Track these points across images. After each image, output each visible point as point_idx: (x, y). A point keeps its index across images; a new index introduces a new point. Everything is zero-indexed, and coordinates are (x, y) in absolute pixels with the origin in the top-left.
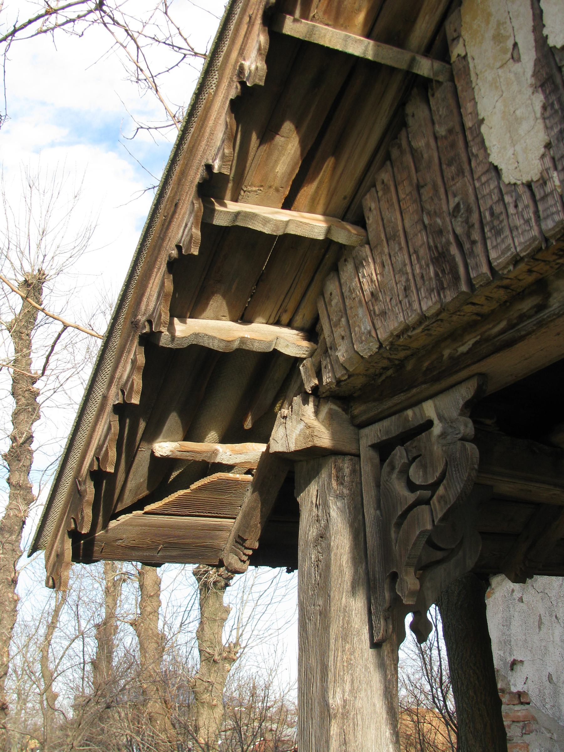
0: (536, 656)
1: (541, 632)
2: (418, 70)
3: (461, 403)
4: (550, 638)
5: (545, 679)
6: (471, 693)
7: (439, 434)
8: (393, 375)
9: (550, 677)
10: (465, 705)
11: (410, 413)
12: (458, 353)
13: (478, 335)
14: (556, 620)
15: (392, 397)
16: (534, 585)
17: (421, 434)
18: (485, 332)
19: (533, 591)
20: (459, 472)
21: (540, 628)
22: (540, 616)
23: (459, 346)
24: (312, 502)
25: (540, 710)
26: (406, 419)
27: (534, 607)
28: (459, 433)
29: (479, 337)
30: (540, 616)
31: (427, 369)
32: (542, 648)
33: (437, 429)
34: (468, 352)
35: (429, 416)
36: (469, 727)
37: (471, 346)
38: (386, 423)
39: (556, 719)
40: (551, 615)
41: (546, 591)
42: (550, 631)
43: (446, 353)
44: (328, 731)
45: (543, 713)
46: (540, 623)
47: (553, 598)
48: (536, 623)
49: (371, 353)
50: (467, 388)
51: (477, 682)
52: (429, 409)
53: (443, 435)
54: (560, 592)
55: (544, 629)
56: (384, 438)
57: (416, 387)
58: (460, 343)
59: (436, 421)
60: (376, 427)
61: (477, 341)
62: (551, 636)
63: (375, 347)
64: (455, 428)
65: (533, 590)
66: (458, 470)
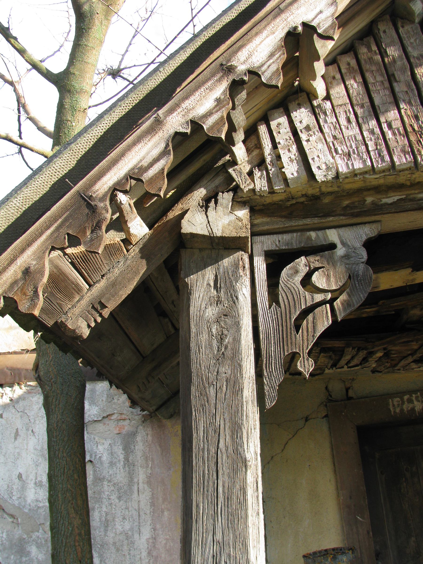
0: (9, 460)
1: (17, 442)
2: (413, 6)
3: (364, 238)
4: (24, 447)
5: (15, 477)
6: (76, 476)
7: (342, 255)
8: (306, 203)
9: (20, 476)
10: (69, 486)
11: (313, 234)
12: (382, 202)
13: (404, 195)
14: (32, 434)
15: (303, 218)
16: (16, 406)
17: (324, 252)
18: (411, 194)
19: (14, 411)
20: (362, 285)
21: (16, 439)
22: (17, 430)
23: (383, 198)
24: (209, 284)
25: (7, 501)
26: (309, 238)
27: (13, 422)
28: (363, 258)
29: (404, 196)
30: (17, 430)
31: (347, 206)
32: (16, 454)
33: (340, 251)
34: (391, 204)
35: (332, 241)
36: (72, 504)
37: (395, 200)
38: (286, 237)
39: (21, 507)
40: (27, 430)
41: (26, 411)
42: (25, 442)
43: (369, 200)
44: (245, 480)
45: (9, 503)
46: (17, 434)
47: (32, 417)
48: (13, 435)
49: (325, 179)
50: (371, 228)
51: (80, 468)
52: (333, 236)
53: (347, 256)
54: (39, 413)
55: (20, 440)
56: (284, 248)
57: (333, 216)
58: (385, 196)
59: (339, 246)
60: (275, 238)
61: (402, 198)
62: (25, 445)
63: (331, 175)
64: (357, 253)
65: (14, 409)
66: (361, 284)
